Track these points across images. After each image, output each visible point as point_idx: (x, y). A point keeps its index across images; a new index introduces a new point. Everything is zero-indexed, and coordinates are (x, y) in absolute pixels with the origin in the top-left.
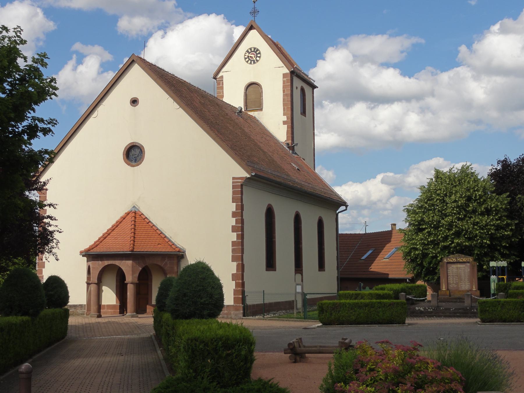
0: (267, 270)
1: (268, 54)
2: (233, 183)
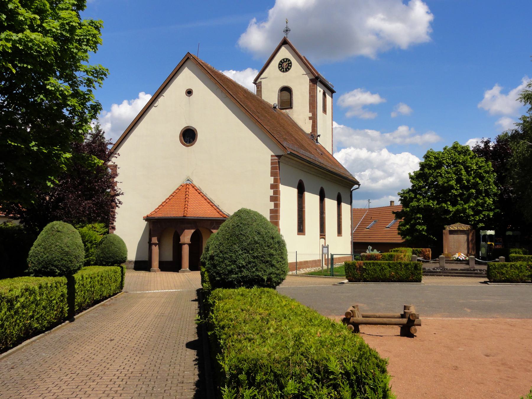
0: (298, 234)
1: (296, 67)
2: (272, 160)
